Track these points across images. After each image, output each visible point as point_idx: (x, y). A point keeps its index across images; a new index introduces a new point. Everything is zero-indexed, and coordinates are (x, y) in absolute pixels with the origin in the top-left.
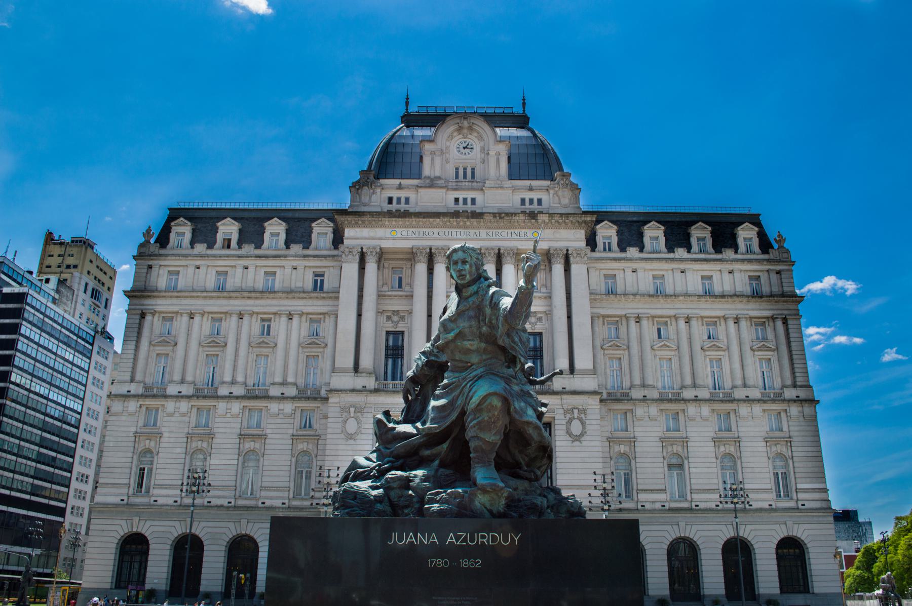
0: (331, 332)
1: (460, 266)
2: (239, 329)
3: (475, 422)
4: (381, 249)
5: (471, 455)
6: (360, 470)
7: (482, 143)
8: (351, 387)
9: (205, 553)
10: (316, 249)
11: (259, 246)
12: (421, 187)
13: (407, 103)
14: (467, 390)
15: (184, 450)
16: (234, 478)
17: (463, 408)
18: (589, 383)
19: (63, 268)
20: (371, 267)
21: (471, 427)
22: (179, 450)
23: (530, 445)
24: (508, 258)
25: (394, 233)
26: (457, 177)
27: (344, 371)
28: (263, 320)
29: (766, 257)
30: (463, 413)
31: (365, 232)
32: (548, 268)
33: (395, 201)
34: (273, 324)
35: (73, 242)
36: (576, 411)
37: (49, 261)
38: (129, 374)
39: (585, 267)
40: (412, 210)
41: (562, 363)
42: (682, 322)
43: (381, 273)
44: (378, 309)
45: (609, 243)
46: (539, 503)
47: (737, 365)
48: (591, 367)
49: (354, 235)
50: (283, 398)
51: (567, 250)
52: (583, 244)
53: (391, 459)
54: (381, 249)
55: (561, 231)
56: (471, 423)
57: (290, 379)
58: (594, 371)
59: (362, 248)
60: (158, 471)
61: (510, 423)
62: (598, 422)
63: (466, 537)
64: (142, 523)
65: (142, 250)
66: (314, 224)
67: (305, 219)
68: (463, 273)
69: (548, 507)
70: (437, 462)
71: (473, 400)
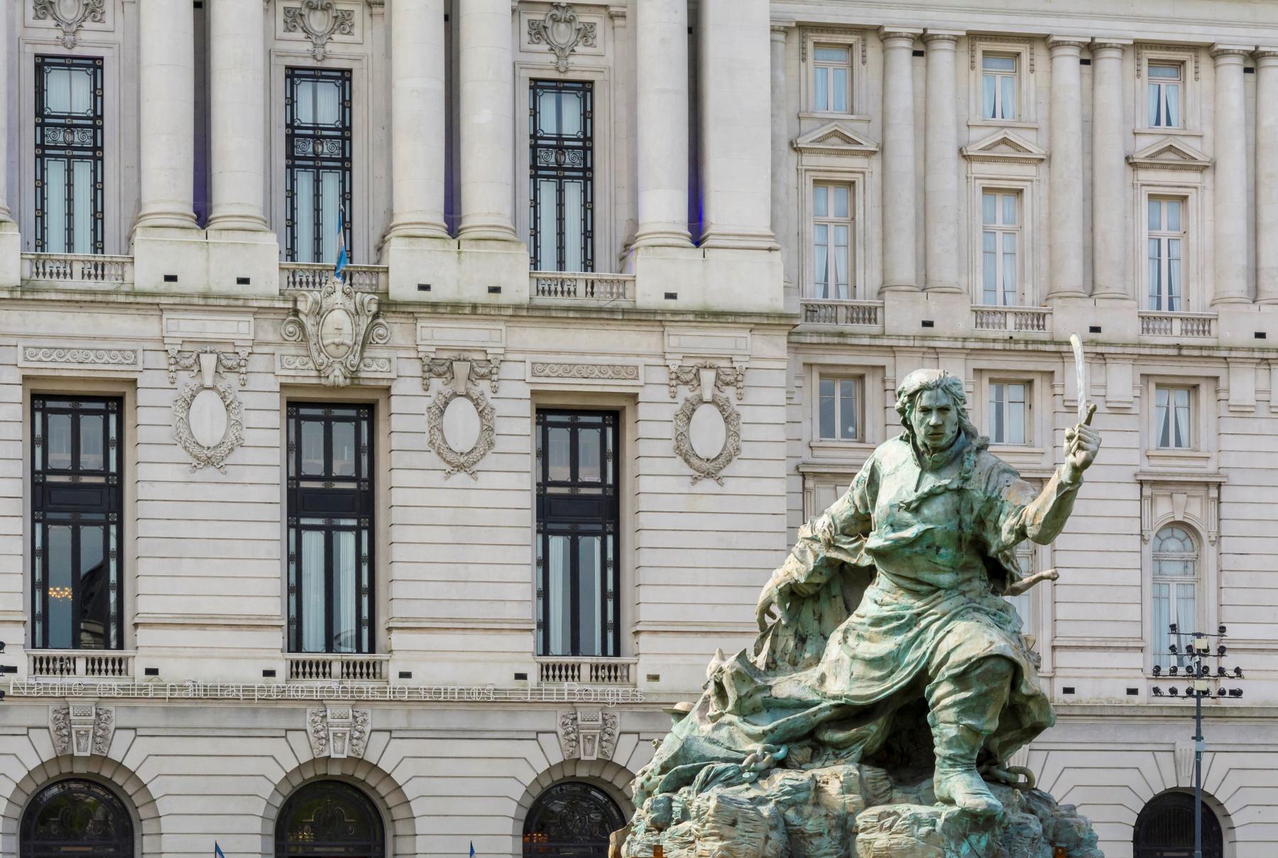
17: (924, 670)
36: (708, 377)
41: (663, 206)
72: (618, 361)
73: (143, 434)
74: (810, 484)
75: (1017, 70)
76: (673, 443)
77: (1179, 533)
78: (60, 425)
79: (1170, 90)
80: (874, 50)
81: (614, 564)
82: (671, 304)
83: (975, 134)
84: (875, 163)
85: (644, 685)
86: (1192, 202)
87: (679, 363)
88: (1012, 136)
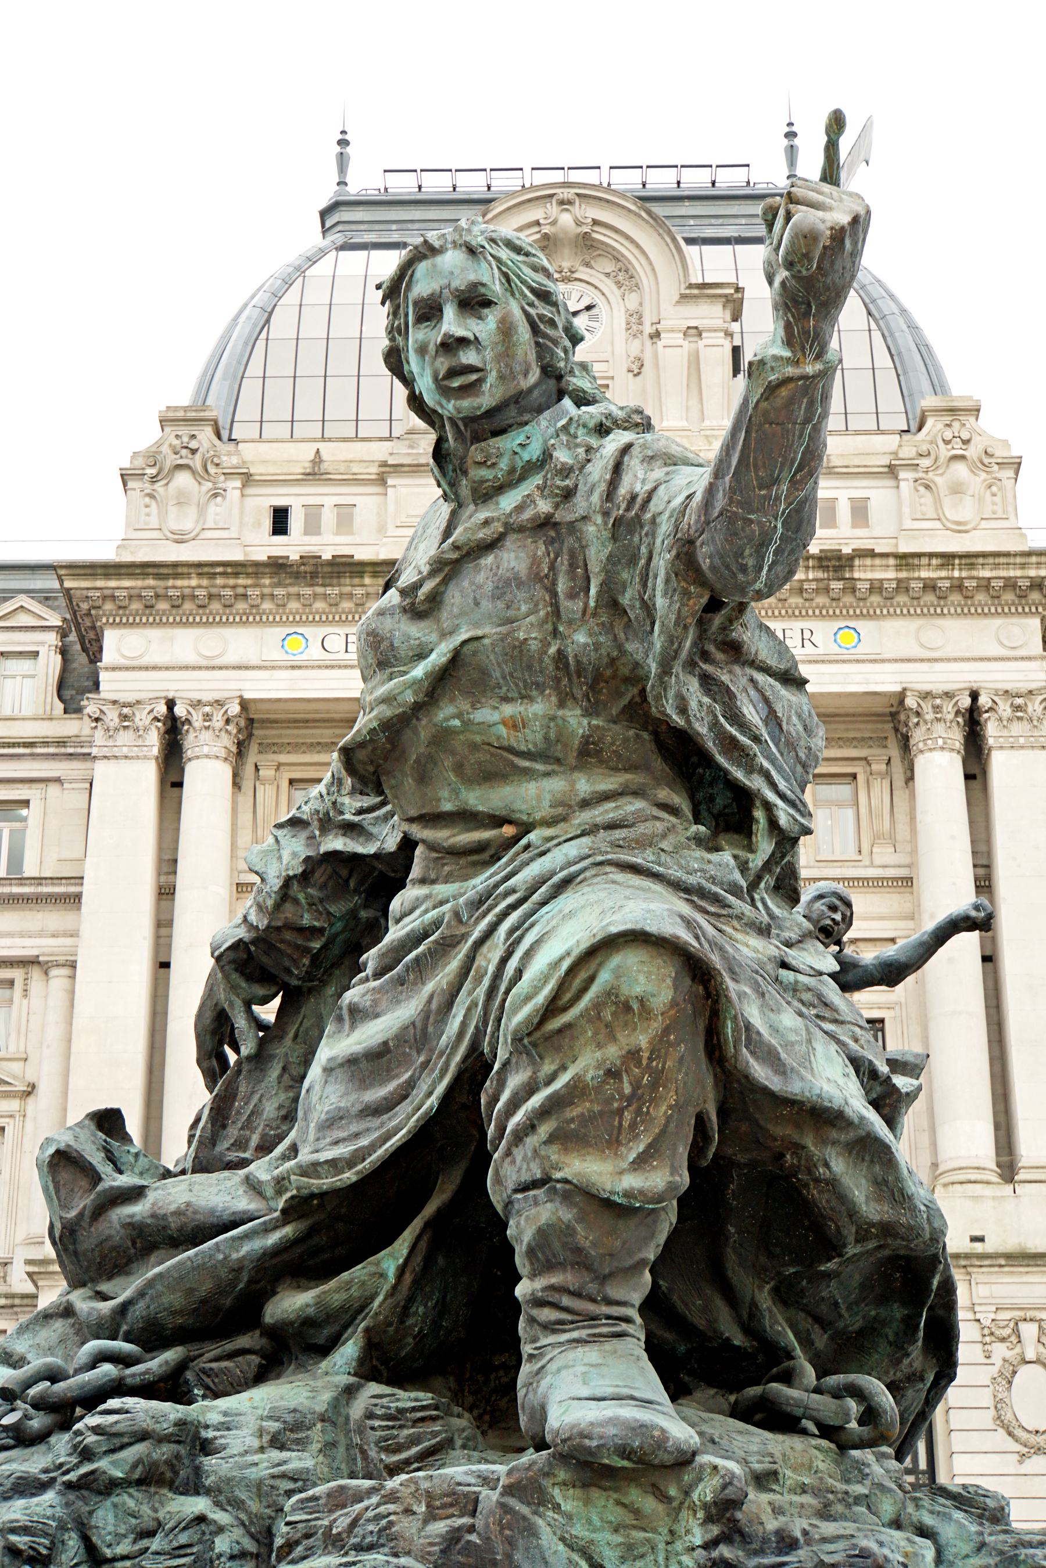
0: (54, 1032)
1: (452, 323)
4: (244, 704)
5: (522, 1290)
7: (632, 301)
13: (342, 161)
17: (475, 1047)
20: (207, 775)
21: (519, 1137)
23: (832, 1247)
25: (295, 644)
30: (475, 1071)
31: (184, 643)
32: (898, 767)
33: (296, 522)
36: (1030, 1331)
40: (361, 555)
43: (245, 800)
49: (143, 660)
54: (244, 704)
55: (948, 623)
56: (514, 1097)
59: (171, 704)
68: (468, 357)
70: (349, 1351)
76: (992, 1412)
82: (978, 1247)
87: (993, 1316)
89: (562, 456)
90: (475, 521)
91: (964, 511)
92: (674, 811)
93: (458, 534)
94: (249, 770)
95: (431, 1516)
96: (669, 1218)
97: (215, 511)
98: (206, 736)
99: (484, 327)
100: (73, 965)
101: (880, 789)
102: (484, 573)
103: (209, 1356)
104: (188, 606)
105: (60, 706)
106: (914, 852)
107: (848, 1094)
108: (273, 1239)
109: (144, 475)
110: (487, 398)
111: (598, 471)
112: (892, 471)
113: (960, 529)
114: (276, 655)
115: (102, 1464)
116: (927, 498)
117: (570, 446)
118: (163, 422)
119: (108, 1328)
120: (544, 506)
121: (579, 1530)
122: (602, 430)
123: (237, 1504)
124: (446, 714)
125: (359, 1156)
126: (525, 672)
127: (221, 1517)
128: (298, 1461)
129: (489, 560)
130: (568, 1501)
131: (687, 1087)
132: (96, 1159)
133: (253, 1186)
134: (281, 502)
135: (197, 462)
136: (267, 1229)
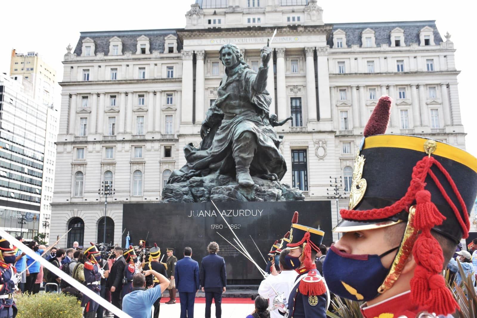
0: (179, 101)
1: (227, 57)
2: (98, 102)
3: (237, 147)
4: (205, 51)
5: (236, 167)
6: (176, 177)
8: (191, 133)
9: (115, 227)
10: (84, 57)
11: (106, 54)
12: (227, 13)
14: (233, 130)
15: (100, 171)
16: (128, 186)
17: (231, 140)
18: (327, 127)
19: (25, 71)
20: (200, 62)
21: (236, 151)
22: (97, 172)
23: (271, 160)
24: (280, 54)
26: (249, 6)
27: (186, 123)
28: (168, 95)
29: (438, 47)
30: (231, 143)
32: (304, 59)
33: (212, 22)
34: (173, 97)
35: (29, 54)
36: (321, 143)
37: (16, 67)
38: (66, 130)
39: (326, 58)
40: (222, 27)
41: (314, 115)
42: (444, 87)
44: (205, 87)
45: (341, 43)
46: (276, 193)
47: (417, 114)
48: (330, 117)
49: (189, 45)
50: (153, 141)
51: (315, 48)
52: (324, 44)
53: (193, 170)
56: (236, 147)
57: (157, 129)
58: (331, 120)
59: (194, 51)
60: (86, 183)
61: (258, 148)
62: (334, 148)
63: (232, 212)
64: (79, 212)
65: (66, 58)
66: (166, 38)
67: (161, 35)
68: (229, 61)
69: (282, 195)
70: (218, 171)
71: (236, 134)
72: (305, 141)
73: (310, 155)
74: (342, 161)
75: (375, 91)
77: (137, 172)
78: (296, 155)
79: (373, 93)
80: (350, 89)
81: (306, 175)
83: (368, 102)
84: (351, 108)
85: (311, 195)
86: (439, 110)
88: (435, 100)
89: (240, 72)
90: (231, 79)
91: (314, 18)
92: (253, 112)
93: (228, 81)
94: (206, 61)
95: (227, 191)
96: (252, 159)
97: (200, 21)
98: (199, 56)
99: (231, 57)
100: (181, 91)
101: (301, 62)
102: (231, 86)
103: (203, 172)
104: (196, 36)
105: (177, 51)
106: (306, 72)
107: (273, 145)
108: (210, 159)
109: (190, 14)
110: (231, 65)
111: (244, 74)
112: (303, 12)
113: (314, 21)
114: (209, 43)
115: (192, 184)
116: (309, 17)
117: (241, 70)
118: (192, 6)
119: (192, 168)
120: (238, 78)
121: (242, 192)
122: (245, 68)
123: (207, 188)
124: (227, 102)
125: (219, 151)
126: (236, 97)
127: (205, 190)
128: (213, 184)
129: (232, 84)
130: (241, 190)
131: (254, 146)
132: (190, 149)
133: (207, 153)
134: (210, 19)
135: (197, 13)
136: (209, 158)
